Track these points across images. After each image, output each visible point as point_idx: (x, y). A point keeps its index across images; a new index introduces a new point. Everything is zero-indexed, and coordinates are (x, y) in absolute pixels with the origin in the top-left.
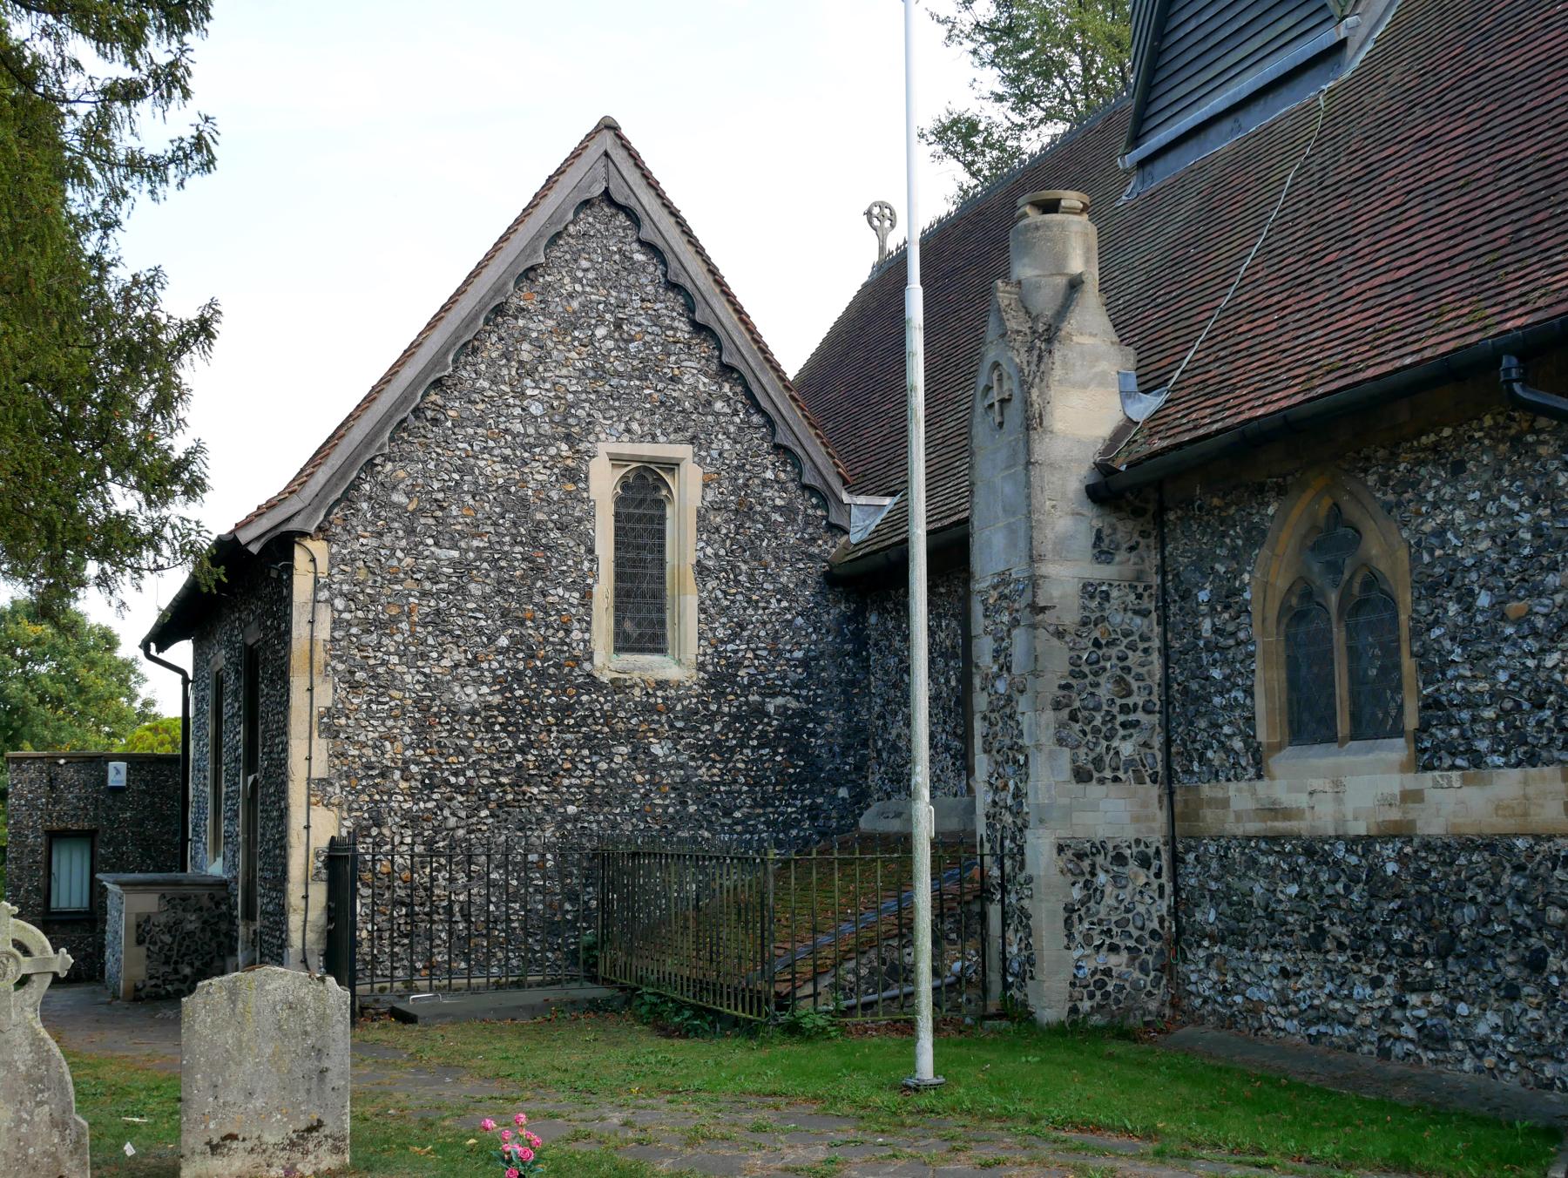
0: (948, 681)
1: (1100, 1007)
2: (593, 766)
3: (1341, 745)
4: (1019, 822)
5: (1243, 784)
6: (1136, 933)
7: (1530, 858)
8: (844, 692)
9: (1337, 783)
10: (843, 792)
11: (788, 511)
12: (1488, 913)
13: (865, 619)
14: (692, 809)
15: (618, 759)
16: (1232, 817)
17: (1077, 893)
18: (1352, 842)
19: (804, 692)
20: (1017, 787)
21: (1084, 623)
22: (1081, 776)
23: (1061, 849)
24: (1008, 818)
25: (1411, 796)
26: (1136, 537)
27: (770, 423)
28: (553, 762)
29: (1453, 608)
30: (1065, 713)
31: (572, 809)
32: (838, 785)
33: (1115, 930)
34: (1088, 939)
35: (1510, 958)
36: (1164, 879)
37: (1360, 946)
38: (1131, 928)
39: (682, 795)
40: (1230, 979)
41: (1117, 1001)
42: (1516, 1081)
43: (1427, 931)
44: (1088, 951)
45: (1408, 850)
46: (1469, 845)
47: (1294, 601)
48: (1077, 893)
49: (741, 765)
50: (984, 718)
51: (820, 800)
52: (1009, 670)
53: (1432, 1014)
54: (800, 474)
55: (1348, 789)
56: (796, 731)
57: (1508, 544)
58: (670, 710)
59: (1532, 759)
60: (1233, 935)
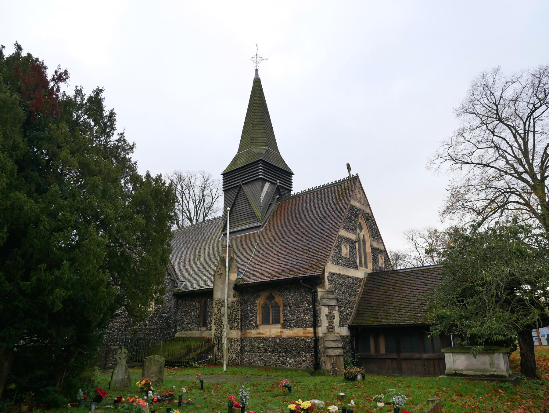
11: (169, 283)
18: (272, 338)
22: (231, 328)
24: (219, 335)
25: (281, 332)
37: (273, 352)
55: (272, 331)
56: (167, 320)
57: (297, 301)
59: (299, 327)
60: (252, 351)
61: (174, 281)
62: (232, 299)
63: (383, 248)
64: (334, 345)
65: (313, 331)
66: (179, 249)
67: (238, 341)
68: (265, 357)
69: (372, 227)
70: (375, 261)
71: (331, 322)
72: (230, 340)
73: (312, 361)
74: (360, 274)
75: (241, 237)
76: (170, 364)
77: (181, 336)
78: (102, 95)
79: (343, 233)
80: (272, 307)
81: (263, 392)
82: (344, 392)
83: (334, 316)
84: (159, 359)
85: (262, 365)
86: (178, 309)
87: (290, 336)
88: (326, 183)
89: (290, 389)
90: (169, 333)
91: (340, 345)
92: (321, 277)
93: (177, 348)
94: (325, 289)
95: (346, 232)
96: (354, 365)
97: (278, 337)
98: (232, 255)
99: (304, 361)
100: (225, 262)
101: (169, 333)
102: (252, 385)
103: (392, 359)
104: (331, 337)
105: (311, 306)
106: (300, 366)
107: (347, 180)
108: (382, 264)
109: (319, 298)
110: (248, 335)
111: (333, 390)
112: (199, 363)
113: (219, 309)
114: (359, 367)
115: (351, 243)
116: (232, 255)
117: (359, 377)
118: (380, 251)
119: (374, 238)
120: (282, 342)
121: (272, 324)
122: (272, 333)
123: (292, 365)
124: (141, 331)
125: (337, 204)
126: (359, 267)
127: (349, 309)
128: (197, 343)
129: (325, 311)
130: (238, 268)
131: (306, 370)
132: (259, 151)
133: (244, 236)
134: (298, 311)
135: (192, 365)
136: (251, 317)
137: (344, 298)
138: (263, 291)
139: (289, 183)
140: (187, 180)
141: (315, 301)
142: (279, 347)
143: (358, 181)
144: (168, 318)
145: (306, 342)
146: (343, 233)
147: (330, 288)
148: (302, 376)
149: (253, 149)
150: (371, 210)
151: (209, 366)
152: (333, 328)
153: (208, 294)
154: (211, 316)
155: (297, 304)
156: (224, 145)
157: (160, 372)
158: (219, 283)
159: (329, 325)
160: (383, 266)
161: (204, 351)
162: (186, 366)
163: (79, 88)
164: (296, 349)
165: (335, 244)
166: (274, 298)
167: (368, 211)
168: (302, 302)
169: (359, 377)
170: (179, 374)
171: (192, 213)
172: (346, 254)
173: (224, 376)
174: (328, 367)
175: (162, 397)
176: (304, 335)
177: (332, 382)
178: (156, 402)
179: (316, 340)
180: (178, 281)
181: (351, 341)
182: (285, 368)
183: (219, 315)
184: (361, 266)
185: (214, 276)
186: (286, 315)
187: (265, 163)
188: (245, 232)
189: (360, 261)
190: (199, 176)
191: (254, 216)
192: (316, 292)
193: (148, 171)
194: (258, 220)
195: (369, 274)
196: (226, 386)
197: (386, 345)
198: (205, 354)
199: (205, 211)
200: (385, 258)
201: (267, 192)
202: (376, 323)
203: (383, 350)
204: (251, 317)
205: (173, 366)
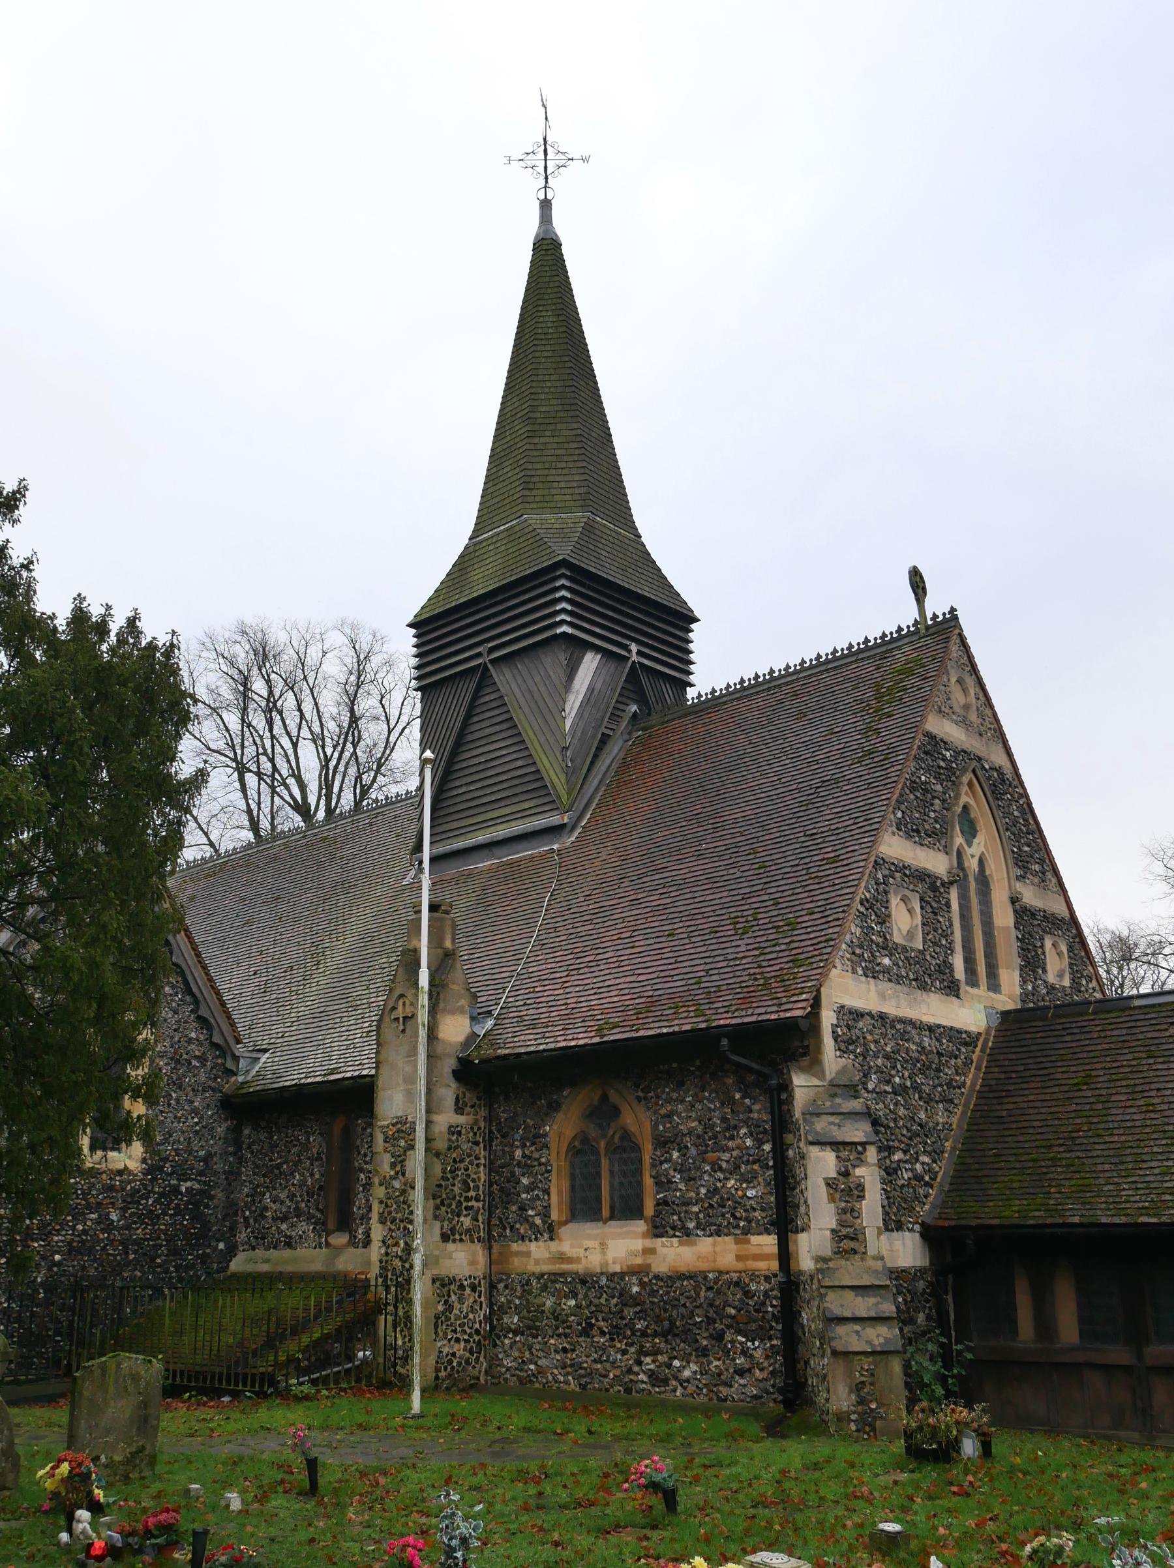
0: (312, 1175)
1: (450, 1375)
2: (74, 1228)
3: (605, 1223)
4: (407, 1265)
5: (541, 1243)
6: (468, 1331)
7: (716, 1283)
8: (227, 1179)
9: (602, 1244)
10: (221, 1246)
11: (202, 1059)
12: (692, 1312)
13: (241, 1131)
14: (132, 1257)
15: (89, 1223)
16: (532, 1262)
17: (440, 1308)
18: (611, 1277)
19: (203, 1179)
20: (406, 1243)
21: (449, 1149)
22: (445, 1238)
23: (434, 1281)
24: (397, 1263)
25: (648, 1251)
26: (475, 1100)
27: (196, 1002)
28: (49, 1224)
29: (675, 1155)
30: (438, 1201)
31: (57, 1257)
32: (218, 1241)
33: (459, 1329)
34: (445, 1334)
35: (705, 1335)
36: (482, 1299)
37: (616, 1332)
38: (466, 1328)
39: (126, 1247)
40: (527, 1354)
41: (458, 1372)
42: (706, 1399)
43: (656, 1323)
44: (445, 1342)
45: (646, 1279)
46: (682, 1277)
47: (577, 1143)
48: (440, 1308)
49: (163, 1227)
50: (381, 1202)
51: (208, 1251)
52: (403, 1174)
53: (658, 1367)
54: (211, 1036)
55: (611, 1247)
56: (196, 1204)
57: (708, 1126)
58: (123, 1189)
59: (718, 1233)
60: (530, 1328)
61: (222, 1050)
62: (446, 1118)
63: (1061, 910)
64: (863, 1306)
65: (775, 1250)
66: (248, 923)
67: (474, 1288)
68: (584, 1355)
69: (1015, 822)
70: (1032, 963)
71: (848, 1213)
72: (443, 1284)
73: (773, 1373)
74: (970, 1014)
75: (488, 869)
76: (189, 1384)
77: (250, 1268)
79: (895, 847)
80: (613, 1150)
81: (564, 1507)
82: (903, 1511)
83: (861, 1187)
84: (144, 1368)
85: (573, 1385)
86: (241, 1160)
88: (825, 650)
89: (670, 1498)
90: (204, 1258)
91: (889, 1309)
92: (804, 1025)
93: (229, 1322)
94: (821, 1075)
95: (908, 844)
96: (949, 1394)
97: (634, 1271)
98: (448, 944)
99: (741, 1372)
100: (418, 965)
101: (205, 1257)
102: (523, 1476)
103: (1108, 1369)
104: (850, 1272)
105: (767, 1147)
106: (724, 1391)
107: (910, 633)
109: (798, 1114)
110: (517, 1263)
111: (859, 1504)
112: (314, 1382)
113: (399, 1162)
114: (969, 1405)
115: (932, 890)
116: (448, 944)
117: (969, 1447)
118: (1050, 922)
119: (1025, 868)
120: (653, 1293)
121: (612, 1217)
122: (610, 1256)
123: (691, 1388)
124: (91, 1251)
125: (870, 730)
126: (964, 988)
127: (927, 1159)
128: (308, 1298)
129: (822, 1165)
130: (474, 996)
131: (751, 1410)
132: (558, 530)
133: (500, 865)
134: (716, 1167)
135: (288, 1388)
136: (528, 1190)
137: (902, 1111)
138: (573, 1084)
139: (681, 657)
140: (287, 661)
141: (781, 1123)
142: (641, 1314)
143: (955, 639)
144: (198, 1199)
145: (748, 1294)
146: (895, 847)
147: (843, 1071)
148: (733, 1437)
149: (533, 519)
151: (358, 1393)
152: (856, 1236)
153: (357, 1097)
154: (368, 1186)
155: (710, 1141)
156: (413, 509)
157: (145, 1423)
158: (395, 1054)
159: (841, 1223)
160: (1066, 982)
161: (338, 1331)
162: (262, 1395)
164: (710, 1321)
165: (861, 893)
166: (617, 1112)
167: (1000, 760)
168: (731, 1129)
169: (969, 1447)
170: (231, 1427)
171: (313, 787)
172: (910, 935)
173: (412, 1434)
174: (839, 1397)
175: (126, 1535)
176: (740, 1266)
177: (852, 1465)
178: (99, 1559)
179: (790, 1284)
180: (239, 1049)
181: (936, 1291)
182: (664, 1404)
183: (397, 1184)
184: (973, 981)
185: (378, 1030)
186: (662, 1183)
187: (579, 575)
188: (505, 849)
189: (969, 961)
190: (337, 639)
191: (537, 788)
192: (786, 1087)
193: (80, 598)
194: (554, 805)
195: (1005, 1014)
196: (414, 1479)
198: (346, 1341)
199: (359, 778)
200: (1071, 949)
201: (591, 690)
202: (1038, 1216)
203: (1068, 1329)
204: (528, 1190)
205: (216, 1393)
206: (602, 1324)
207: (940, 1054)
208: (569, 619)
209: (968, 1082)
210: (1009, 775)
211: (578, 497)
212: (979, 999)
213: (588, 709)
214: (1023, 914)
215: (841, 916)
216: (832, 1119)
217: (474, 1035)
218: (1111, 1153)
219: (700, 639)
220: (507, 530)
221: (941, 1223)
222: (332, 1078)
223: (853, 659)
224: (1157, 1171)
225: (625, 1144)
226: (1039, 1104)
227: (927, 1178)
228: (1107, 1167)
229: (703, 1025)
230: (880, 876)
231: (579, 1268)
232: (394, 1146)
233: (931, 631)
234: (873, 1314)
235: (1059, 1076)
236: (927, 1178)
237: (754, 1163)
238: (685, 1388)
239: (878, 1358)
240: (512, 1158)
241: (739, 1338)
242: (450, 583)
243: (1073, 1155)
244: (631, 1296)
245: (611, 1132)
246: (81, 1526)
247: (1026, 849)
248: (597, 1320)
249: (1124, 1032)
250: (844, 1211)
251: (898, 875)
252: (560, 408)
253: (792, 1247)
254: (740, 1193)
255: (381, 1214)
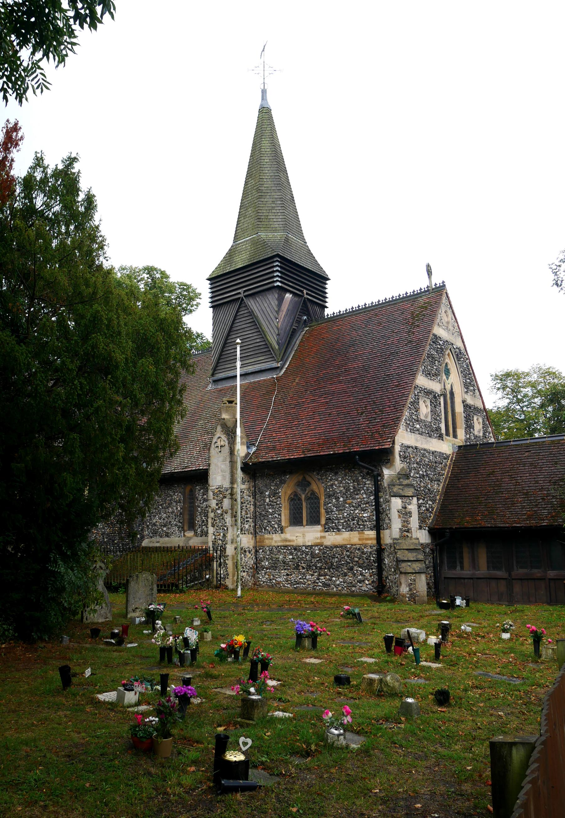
3: (304, 526)
5: (277, 535)
18: (307, 547)
20: (224, 535)
25: (322, 537)
37: (309, 567)
46: (336, 547)
50: (212, 519)
52: (222, 508)
55: (308, 535)
57: (348, 489)
60: (274, 567)
65: (375, 536)
70: (469, 427)
71: (406, 523)
73: (373, 582)
78: (77, 167)
83: (410, 513)
87: (337, 544)
91: (421, 557)
99: (360, 581)
105: (372, 498)
107: (425, 291)
108: (479, 432)
110: (267, 542)
127: (431, 503)
138: (291, 473)
139: (322, 295)
141: (378, 489)
146: (421, 381)
150: (463, 342)
160: (481, 434)
163: (39, 155)
166: (309, 484)
167: (459, 344)
172: (426, 416)
176: (361, 542)
184: (447, 434)
187: (284, 261)
192: (381, 474)
195: (460, 447)
197: (488, 558)
200: (483, 421)
206: (303, 565)
207: (436, 462)
208: (280, 280)
209: (446, 474)
210: (463, 351)
211: (281, 226)
212: (450, 441)
213: (287, 318)
214: (466, 406)
215: (402, 408)
216: (400, 487)
217: (248, 454)
218: (502, 500)
219: (330, 287)
220: (251, 239)
221: (436, 527)
222: (186, 470)
223: (401, 301)
224: (520, 507)
225: (312, 496)
226: (474, 482)
227: (430, 510)
228: (500, 506)
229: (348, 451)
230: (416, 392)
231: (294, 544)
232: (217, 497)
233: (434, 291)
234: (415, 559)
235: (482, 471)
236: (430, 510)
237: (366, 504)
238: (337, 588)
239: (417, 575)
240: (265, 501)
241: (360, 569)
242: (225, 262)
243: (487, 501)
244: (316, 554)
245: (307, 492)
246: (158, 626)
247: (468, 381)
248: (301, 563)
249: (507, 455)
250: (404, 521)
251: (422, 392)
252: (273, 185)
253: (382, 536)
254: (361, 515)
255: (213, 523)
